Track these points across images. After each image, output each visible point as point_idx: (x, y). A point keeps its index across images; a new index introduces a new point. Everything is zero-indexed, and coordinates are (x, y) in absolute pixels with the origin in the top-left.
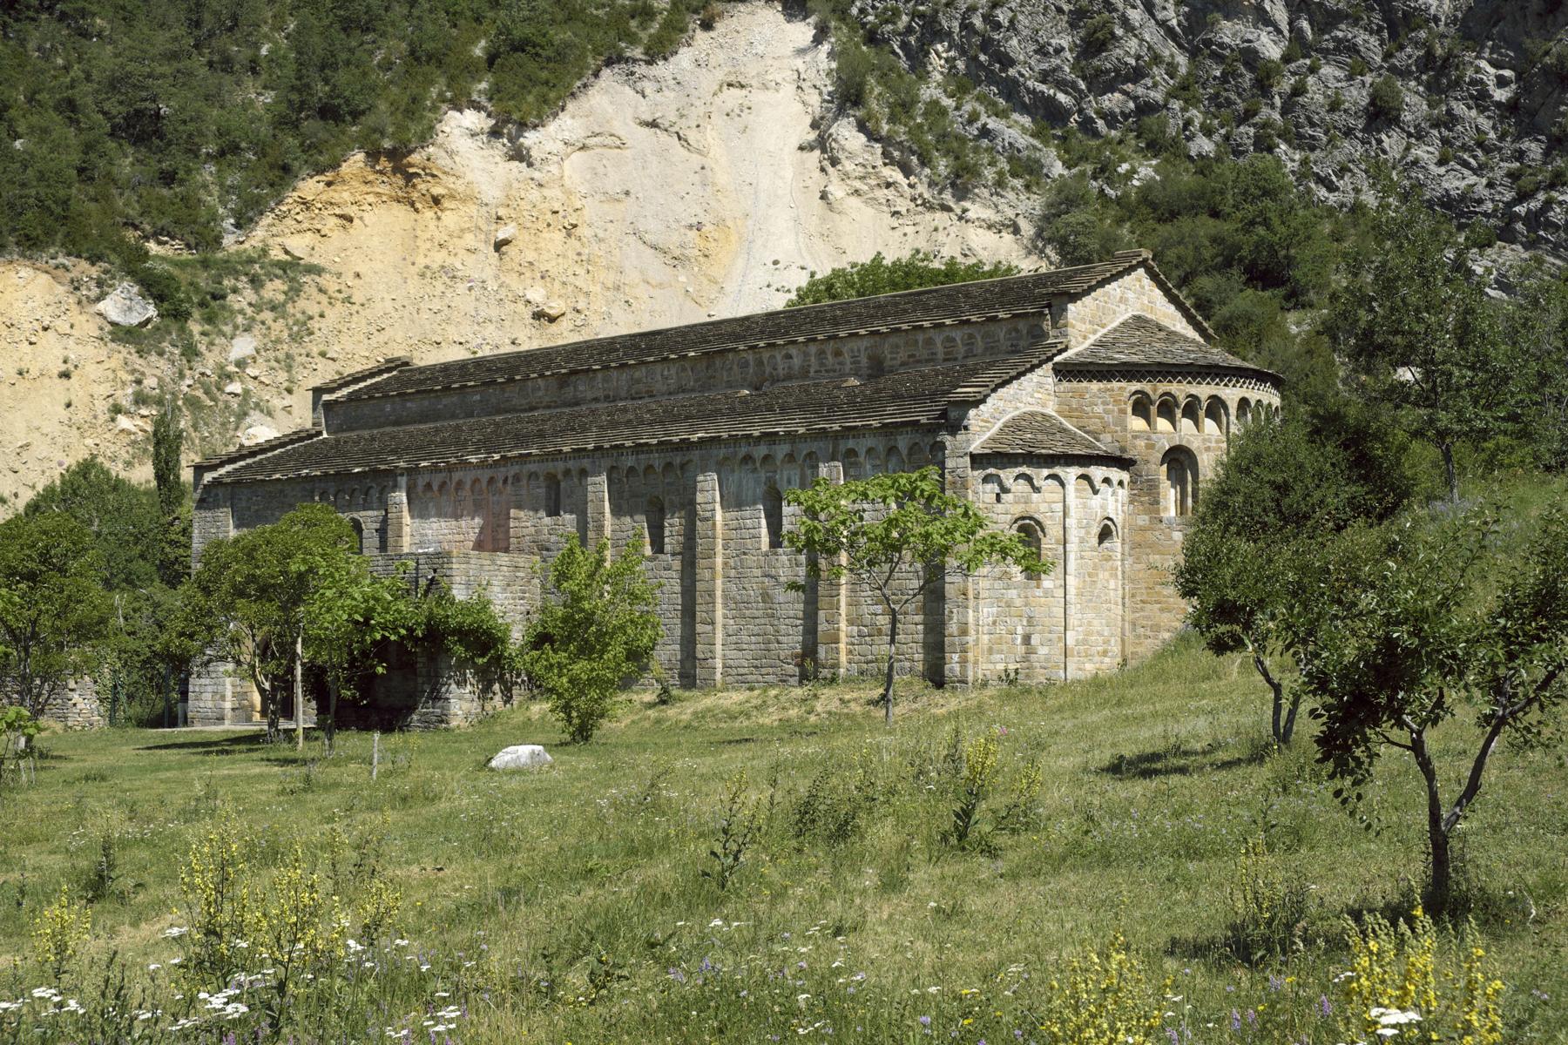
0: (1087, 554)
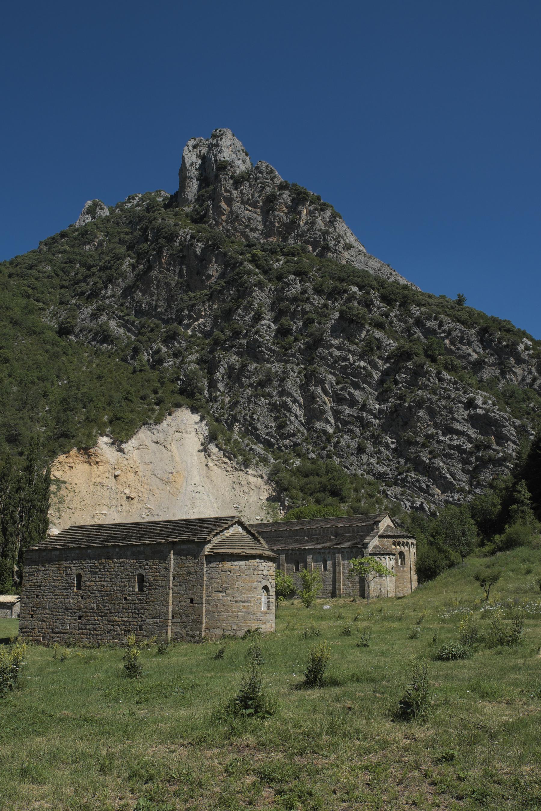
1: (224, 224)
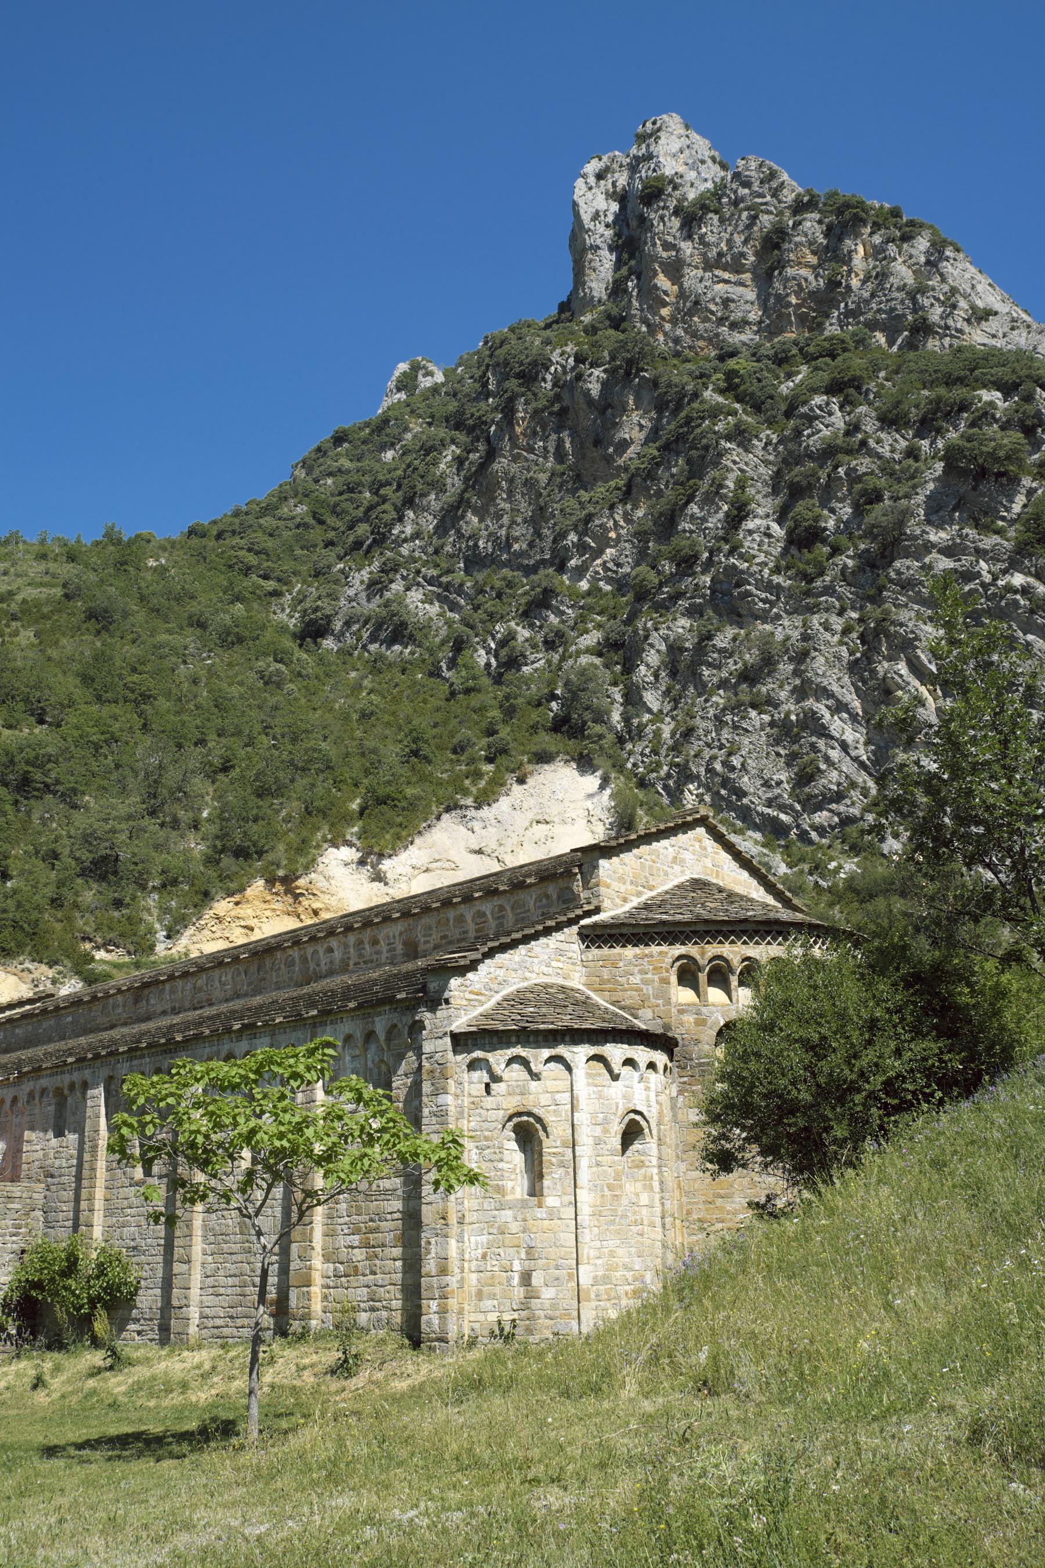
0: (606, 1160)
1: (668, 326)
